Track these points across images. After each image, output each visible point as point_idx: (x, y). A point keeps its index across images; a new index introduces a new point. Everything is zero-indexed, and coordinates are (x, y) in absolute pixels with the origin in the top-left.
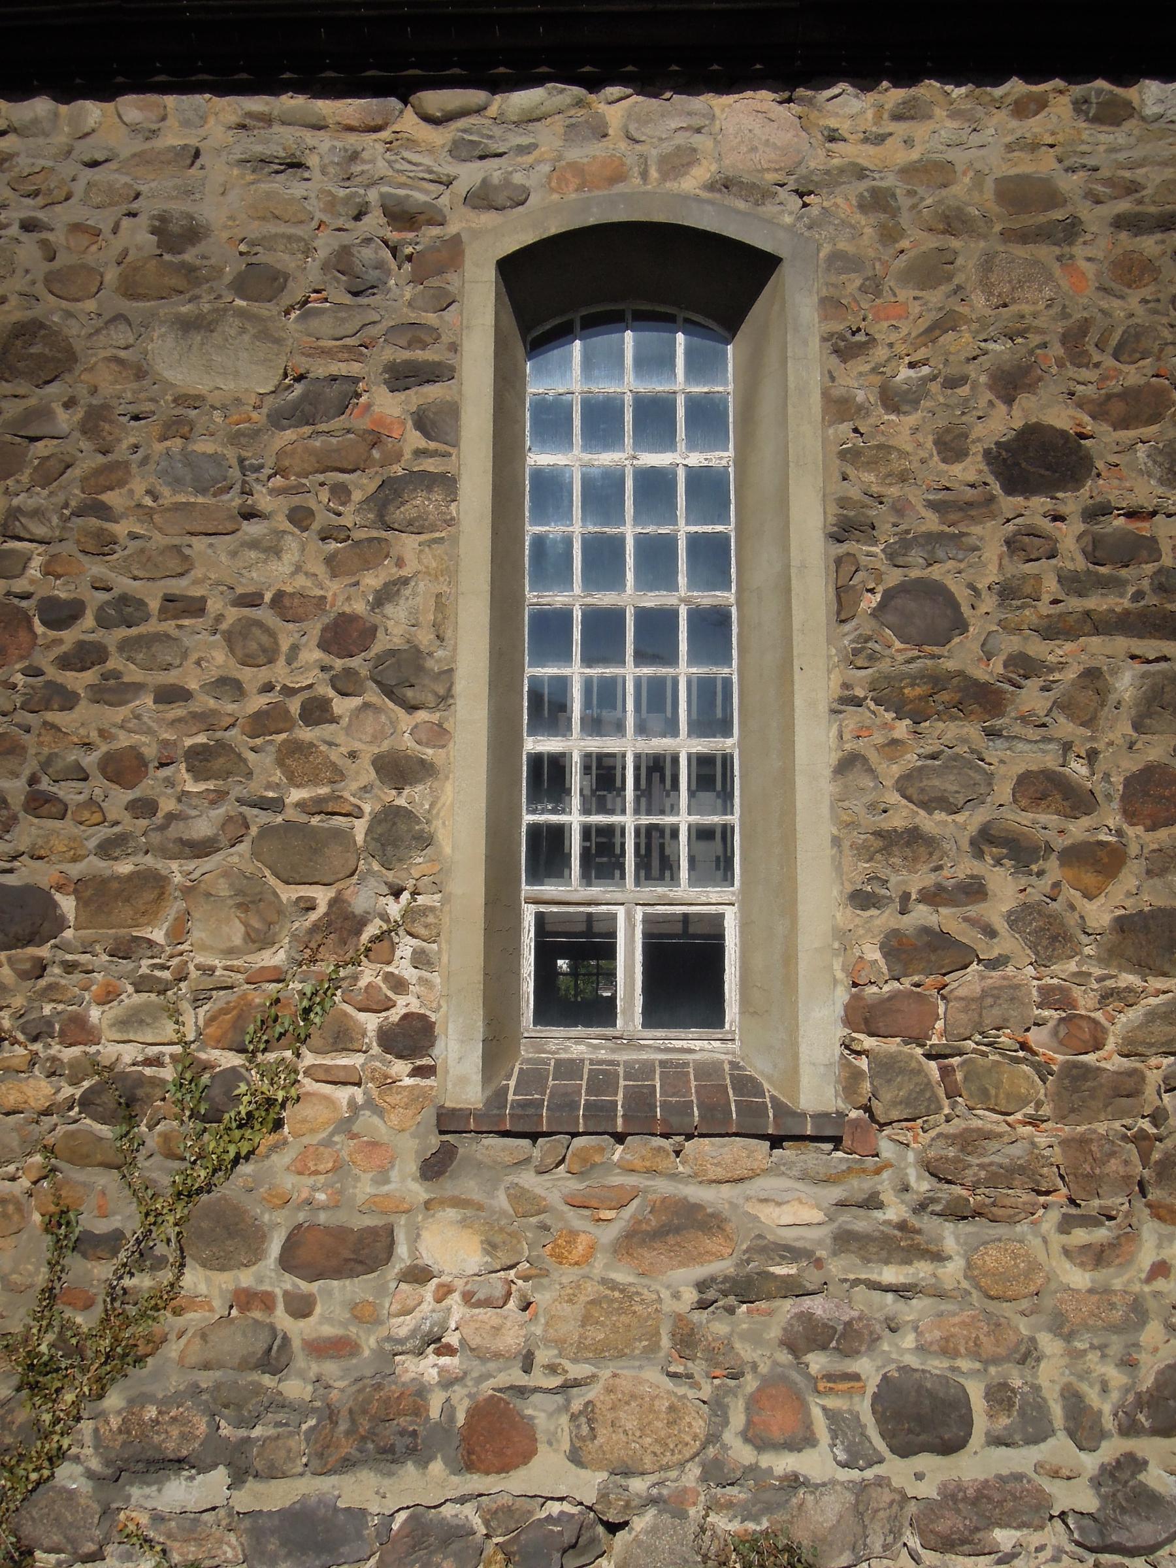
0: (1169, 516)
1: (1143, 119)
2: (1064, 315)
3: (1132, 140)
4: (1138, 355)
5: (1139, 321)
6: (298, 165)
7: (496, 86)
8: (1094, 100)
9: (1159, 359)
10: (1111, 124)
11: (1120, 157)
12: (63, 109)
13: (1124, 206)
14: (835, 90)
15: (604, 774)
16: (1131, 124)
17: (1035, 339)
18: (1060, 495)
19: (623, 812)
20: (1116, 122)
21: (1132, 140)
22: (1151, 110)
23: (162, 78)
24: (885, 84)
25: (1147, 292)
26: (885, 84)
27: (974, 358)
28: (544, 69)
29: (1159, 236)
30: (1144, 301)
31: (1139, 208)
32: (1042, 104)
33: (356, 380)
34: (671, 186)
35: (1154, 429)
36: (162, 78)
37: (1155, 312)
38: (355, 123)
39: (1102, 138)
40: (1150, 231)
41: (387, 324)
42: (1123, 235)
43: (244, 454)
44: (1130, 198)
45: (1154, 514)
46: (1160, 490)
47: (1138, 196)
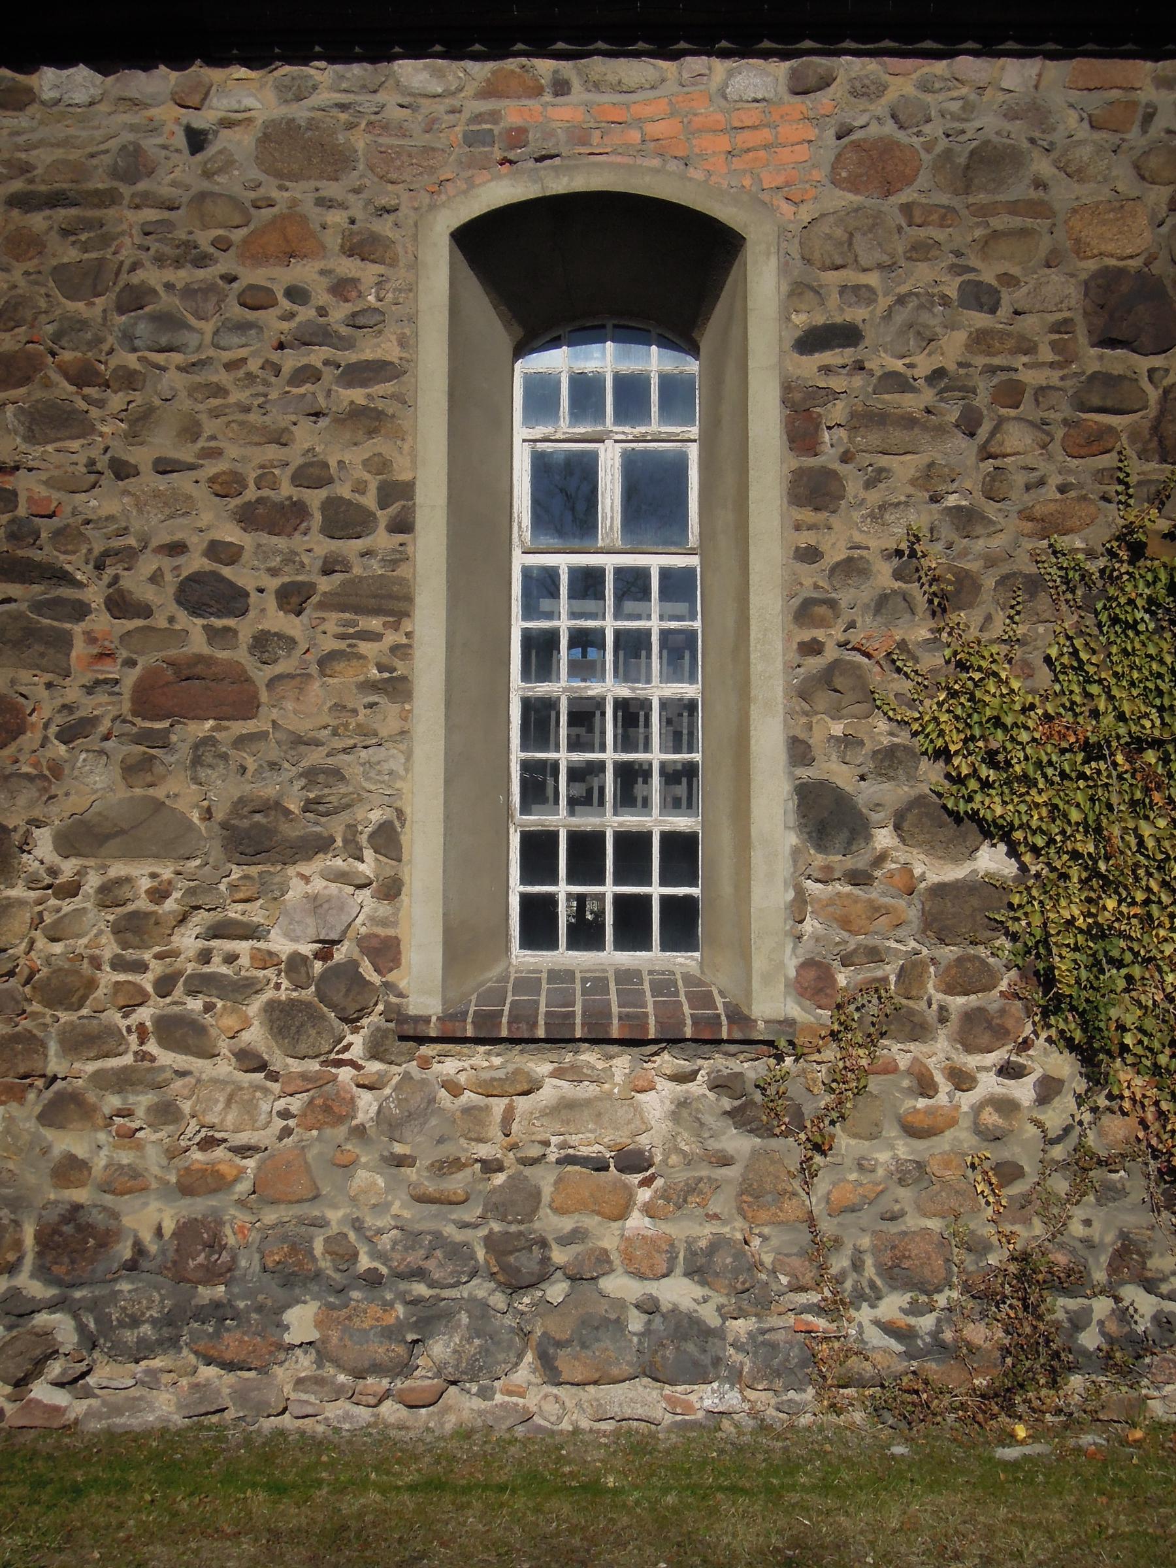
0: (30, 470)
1: (43, 103)
3: (35, 123)
4: (12, 324)
5: (20, 291)
9: (32, 327)
10: (15, 109)
11: (20, 140)
13: (17, 185)
15: (631, 714)
16: (33, 109)
19: (557, 750)
20: (20, 107)
21: (35, 123)
22: (48, 95)
25: (30, 265)
28: (683, 45)
29: (47, 212)
30: (27, 273)
31: (31, 187)
35: (22, 390)
37: (37, 283)
40: (39, 208)
42: (15, 213)
44: (23, 178)
45: (17, 468)
46: (23, 447)
47: (29, 175)
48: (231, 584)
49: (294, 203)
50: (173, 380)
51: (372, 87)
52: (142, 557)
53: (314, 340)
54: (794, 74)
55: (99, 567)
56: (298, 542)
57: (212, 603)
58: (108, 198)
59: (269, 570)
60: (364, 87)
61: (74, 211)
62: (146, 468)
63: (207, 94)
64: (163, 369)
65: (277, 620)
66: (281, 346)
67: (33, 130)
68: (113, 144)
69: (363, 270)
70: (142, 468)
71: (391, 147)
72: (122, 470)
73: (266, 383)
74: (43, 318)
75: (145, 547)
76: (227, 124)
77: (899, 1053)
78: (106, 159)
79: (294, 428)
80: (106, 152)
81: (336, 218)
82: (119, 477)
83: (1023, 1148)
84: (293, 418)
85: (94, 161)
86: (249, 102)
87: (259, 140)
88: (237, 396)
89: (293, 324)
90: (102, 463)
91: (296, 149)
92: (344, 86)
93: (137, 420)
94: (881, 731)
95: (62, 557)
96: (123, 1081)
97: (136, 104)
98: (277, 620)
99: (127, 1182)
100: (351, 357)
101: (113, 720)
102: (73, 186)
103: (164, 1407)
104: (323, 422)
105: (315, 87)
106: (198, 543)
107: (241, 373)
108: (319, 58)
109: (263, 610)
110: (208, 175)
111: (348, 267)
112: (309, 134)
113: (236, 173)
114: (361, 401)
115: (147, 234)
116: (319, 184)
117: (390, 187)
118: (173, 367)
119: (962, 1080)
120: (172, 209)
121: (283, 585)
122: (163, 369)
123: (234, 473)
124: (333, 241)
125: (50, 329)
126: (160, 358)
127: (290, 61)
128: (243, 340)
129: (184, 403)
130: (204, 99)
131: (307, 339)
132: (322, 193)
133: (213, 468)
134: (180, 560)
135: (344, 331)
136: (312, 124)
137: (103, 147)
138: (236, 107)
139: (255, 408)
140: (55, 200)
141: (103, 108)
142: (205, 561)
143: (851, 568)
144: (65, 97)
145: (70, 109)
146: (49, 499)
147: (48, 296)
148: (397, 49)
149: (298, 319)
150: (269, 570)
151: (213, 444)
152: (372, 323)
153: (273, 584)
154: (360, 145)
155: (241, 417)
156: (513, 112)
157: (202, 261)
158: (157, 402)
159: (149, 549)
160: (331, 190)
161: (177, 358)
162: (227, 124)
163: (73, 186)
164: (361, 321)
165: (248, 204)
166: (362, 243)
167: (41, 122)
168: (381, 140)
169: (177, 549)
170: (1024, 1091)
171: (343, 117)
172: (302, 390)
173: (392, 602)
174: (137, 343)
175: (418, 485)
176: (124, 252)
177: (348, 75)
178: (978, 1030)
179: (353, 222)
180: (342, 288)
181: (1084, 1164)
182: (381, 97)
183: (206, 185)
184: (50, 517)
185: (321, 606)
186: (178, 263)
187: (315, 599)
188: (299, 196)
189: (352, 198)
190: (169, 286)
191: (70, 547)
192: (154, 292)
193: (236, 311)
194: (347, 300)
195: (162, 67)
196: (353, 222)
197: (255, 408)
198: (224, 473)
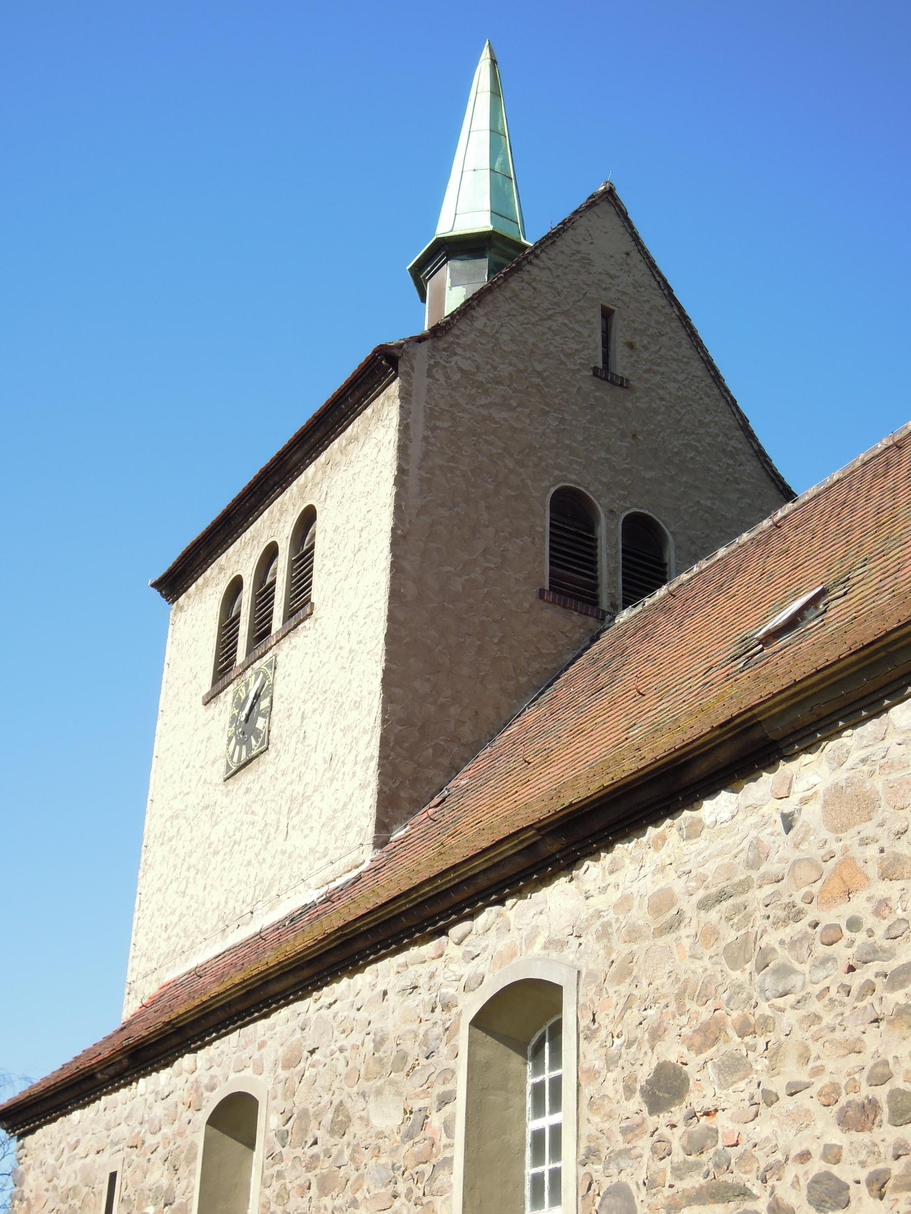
2: (677, 980)
4: (705, 999)
6: (416, 987)
7: (472, 916)
8: (684, 826)
10: (695, 837)
12: (352, 981)
13: (701, 894)
14: (585, 867)
17: (663, 1002)
18: (673, 1109)
20: (697, 834)
23: (372, 957)
24: (603, 854)
26: (603, 854)
27: (641, 1024)
31: (708, 892)
32: (663, 838)
33: (426, 1109)
34: (530, 952)
36: (372, 957)
38: (433, 956)
39: (693, 848)
40: (713, 906)
41: (438, 1071)
43: (395, 1161)
45: (716, 1111)
48: (838, 1180)
49: (846, 849)
50: (790, 1018)
51: (881, 736)
52: (787, 1167)
53: (869, 958)
54: (830, 760)
55: (764, 1181)
56: (877, 1134)
57: (827, 1199)
58: (745, 886)
59: (860, 1163)
61: (731, 901)
62: (782, 1094)
63: (790, 784)
64: (783, 1010)
66: (851, 969)
67: (707, 848)
68: (746, 844)
69: (891, 888)
70: (780, 1095)
71: (895, 781)
72: (770, 1099)
73: (843, 1004)
74: (721, 989)
75: (787, 1159)
76: (805, 801)
78: (742, 856)
79: (864, 1037)
80: (743, 850)
81: (872, 851)
82: (770, 1104)
84: (862, 1028)
85: (737, 860)
86: (814, 779)
87: (824, 807)
88: (828, 1019)
89: (854, 949)
90: (758, 1098)
91: (849, 804)
92: (865, 743)
93: (773, 1056)
95: (745, 1177)
97: (754, 807)
100: (891, 966)
102: (728, 882)
104: (883, 1024)
105: (848, 752)
106: (816, 1150)
107: (826, 1000)
108: (845, 729)
109: (860, 1199)
110: (797, 846)
111: (883, 889)
112: (849, 789)
113: (812, 838)
114: (903, 1001)
115: (767, 906)
116: (858, 828)
117: (902, 812)
118: (788, 1008)
120: (779, 881)
121: (871, 1174)
122: (783, 1010)
123: (833, 1084)
124: (873, 870)
125: (725, 996)
126: (780, 1002)
127: (829, 738)
128: (825, 973)
129: (799, 1035)
130: (790, 788)
131: (864, 958)
132: (862, 835)
133: (820, 1083)
134: (808, 1165)
135: (887, 944)
136: (850, 782)
137: (740, 847)
138: (807, 787)
139: (838, 1027)
140: (721, 896)
141: (739, 817)
142: (823, 1163)
144: (718, 818)
145: (723, 825)
146: (733, 1132)
147: (722, 971)
148: (887, 702)
149: (856, 944)
150: (860, 1163)
151: (818, 1063)
152: (900, 933)
153: (863, 1175)
154: (879, 787)
155: (830, 1036)
157: (798, 916)
158: (783, 1038)
159: (790, 1160)
160: (869, 829)
161: (791, 999)
162: (805, 801)
163: (728, 882)
164: (894, 933)
165: (820, 861)
166: (891, 865)
167: (711, 841)
168: (890, 778)
169: (805, 1156)
171: (866, 768)
172: (864, 1003)
174: (768, 994)
175: (455, 1158)
176: (757, 924)
177: (865, 734)
179: (882, 851)
180: (882, 907)
182: (886, 743)
183: (798, 855)
184: (736, 1145)
185: (896, 1188)
186: (785, 922)
187: (890, 1184)
188: (848, 843)
189: (879, 831)
190: (782, 942)
191: (747, 1168)
192: (773, 950)
193: (821, 950)
194: (884, 918)
195: (764, 774)
196: (882, 851)
197: (838, 1027)
198: (826, 1086)
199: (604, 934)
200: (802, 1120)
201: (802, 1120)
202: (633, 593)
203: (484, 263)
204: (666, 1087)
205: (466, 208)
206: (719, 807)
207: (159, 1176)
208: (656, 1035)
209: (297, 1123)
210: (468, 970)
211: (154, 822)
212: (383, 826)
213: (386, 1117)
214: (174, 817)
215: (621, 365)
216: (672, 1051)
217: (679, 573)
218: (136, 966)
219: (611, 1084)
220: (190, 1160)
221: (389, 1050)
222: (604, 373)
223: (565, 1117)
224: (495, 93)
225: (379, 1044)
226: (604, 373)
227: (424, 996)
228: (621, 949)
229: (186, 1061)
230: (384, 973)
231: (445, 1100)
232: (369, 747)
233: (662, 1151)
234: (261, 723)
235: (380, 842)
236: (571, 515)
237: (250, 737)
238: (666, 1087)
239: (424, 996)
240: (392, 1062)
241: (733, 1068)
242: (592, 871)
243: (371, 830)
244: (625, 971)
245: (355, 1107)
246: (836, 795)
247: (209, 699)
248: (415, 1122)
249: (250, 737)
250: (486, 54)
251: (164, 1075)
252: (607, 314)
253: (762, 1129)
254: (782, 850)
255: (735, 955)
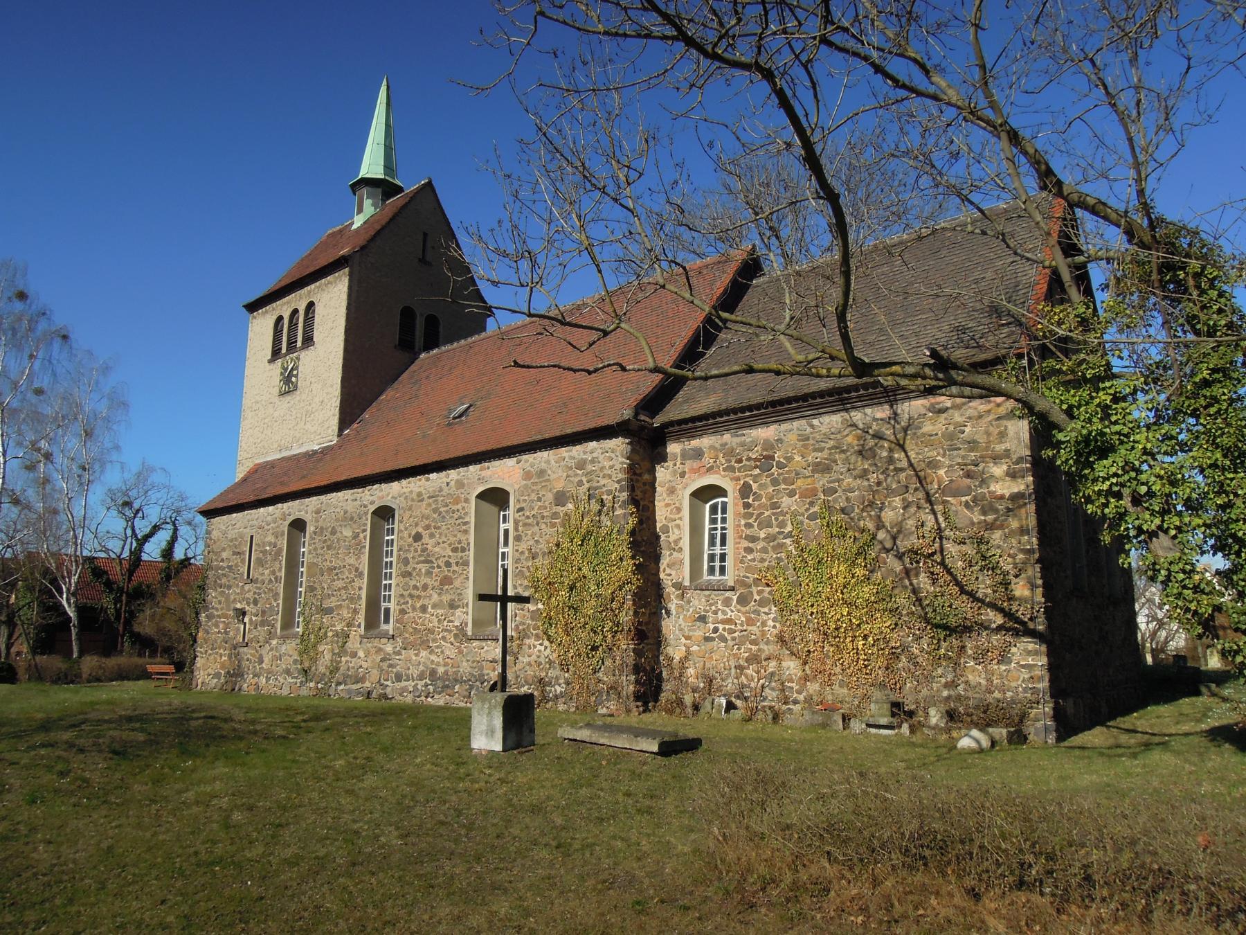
60: (941, 364)
65: (455, 568)
77: (527, 641)
83: (542, 660)
94: (526, 583)
96: (437, 647)
98: (455, 568)
99: (438, 664)
101: (1160, 272)
103: (441, 703)
119: (535, 647)
143: (522, 553)
156: (484, 473)
170: (542, 648)
173: (466, 563)
178: (537, 637)
181: (550, 662)
199: (406, 498)
200: (444, 549)
201: (444, 549)
202: (428, 347)
203: (380, 190)
204: (418, 537)
205: (372, 165)
206: (433, 476)
207: (271, 538)
208: (417, 525)
209: (320, 531)
210: (371, 498)
211: (247, 402)
212: (341, 430)
213: (348, 533)
214: (257, 402)
215: (428, 258)
216: (420, 530)
217: (444, 344)
218: (242, 455)
219: (406, 534)
220: (283, 534)
221: (348, 515)
222: (423, 261)
223: (393, 582)
224: (388, 104)
225: (346, 512)
226: (423, 261)
227: (358, 502)
228: (410, 503)
229: (280, 505)
230: (347, 494)
231: (364, 531)
232: (336, 402)
233: (416, 551)
234: (293, 379)
235: (339, 435)
236: (408, 315)
237: (289, 382)
238: (418, 537)
239: (358, 502)
240: (348, 519)
241: (432, 536)
242: (404, 482)
243: (336, 428)
244: (410, 509)
245: (339, 529)
246: (457, 481)
247: (271, 361)
248: (356, 536)
249: (289, 382)
250: (385, 82)
251: (271, 508)
252: (425, 235)
253: (437, 549)
254: (446, 489)
255: (435, 511)
